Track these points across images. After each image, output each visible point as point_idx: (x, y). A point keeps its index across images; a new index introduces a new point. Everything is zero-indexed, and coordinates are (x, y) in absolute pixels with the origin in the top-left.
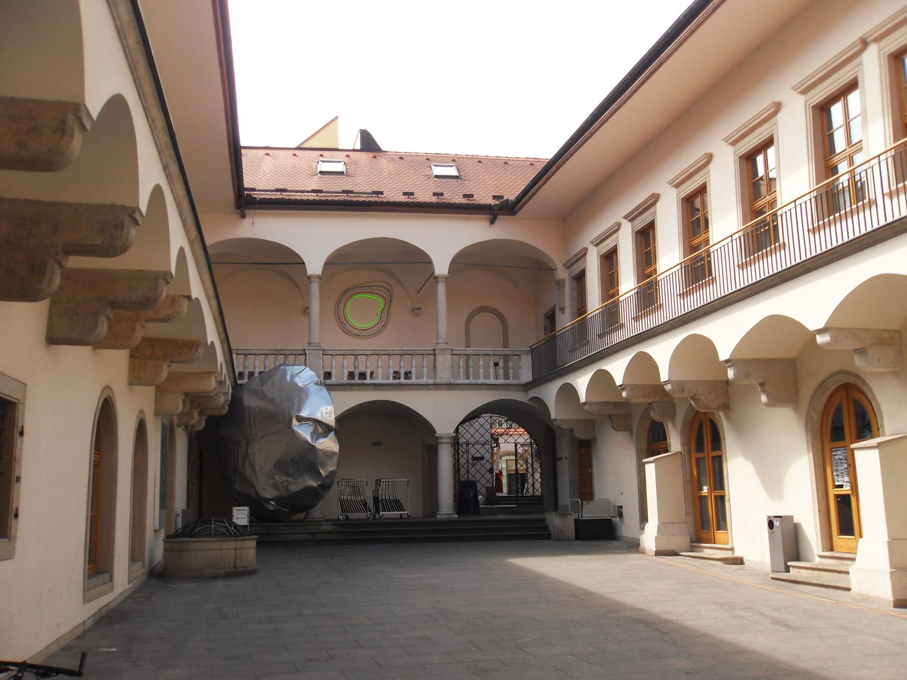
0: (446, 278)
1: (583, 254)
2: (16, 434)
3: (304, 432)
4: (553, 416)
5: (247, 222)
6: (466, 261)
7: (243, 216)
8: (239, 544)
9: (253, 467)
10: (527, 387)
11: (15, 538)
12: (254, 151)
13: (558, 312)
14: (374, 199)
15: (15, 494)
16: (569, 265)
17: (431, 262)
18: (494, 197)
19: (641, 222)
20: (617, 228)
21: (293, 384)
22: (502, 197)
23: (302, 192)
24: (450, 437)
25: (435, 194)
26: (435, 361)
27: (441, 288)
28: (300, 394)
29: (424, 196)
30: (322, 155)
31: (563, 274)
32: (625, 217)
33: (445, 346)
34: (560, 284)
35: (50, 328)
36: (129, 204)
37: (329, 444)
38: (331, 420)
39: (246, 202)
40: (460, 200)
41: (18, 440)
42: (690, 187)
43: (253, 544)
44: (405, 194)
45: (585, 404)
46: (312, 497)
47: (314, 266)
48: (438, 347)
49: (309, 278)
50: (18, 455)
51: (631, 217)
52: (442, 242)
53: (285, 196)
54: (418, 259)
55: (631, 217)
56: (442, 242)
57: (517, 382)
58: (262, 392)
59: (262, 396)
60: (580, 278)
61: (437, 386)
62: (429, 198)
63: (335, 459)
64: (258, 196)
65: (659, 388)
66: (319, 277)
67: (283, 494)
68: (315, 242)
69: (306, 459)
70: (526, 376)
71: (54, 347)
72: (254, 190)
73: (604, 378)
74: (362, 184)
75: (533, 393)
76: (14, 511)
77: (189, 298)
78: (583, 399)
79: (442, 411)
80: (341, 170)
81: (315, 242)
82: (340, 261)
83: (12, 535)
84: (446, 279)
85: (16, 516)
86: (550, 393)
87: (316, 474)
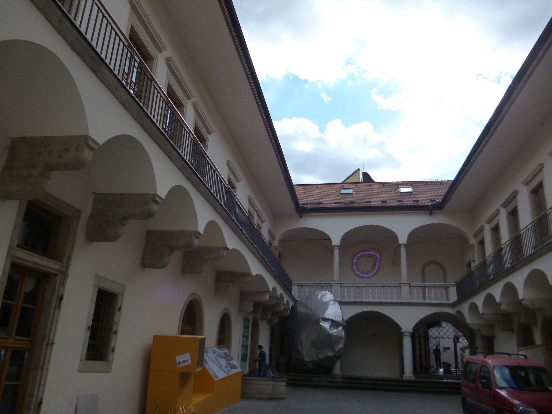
0: (405, 245)
1: (482, 229)
2: (117, 310)
3: (326, 325)
4: (468, 322)
5: (303, 220)
6: (415, 236)
7: (301, 217)
8: (275, 383)
9: (301, 344)
10: (454, 305)
11: (112, 362)
12: (311, 186)
13: (472, 262)
14: (366, 205)
15: (113, 340)
16: (476, 236)
17: (397, 237)
18: (431, 201)
19: (510, 207)
20: (497, 213)
21: (321, 300)
22: (435, 201)
23: (330, 204)
24: (410, 333)
25: (398, 201)
26: (400, 290)
27: (403, 251)
28: (325, 305)
29: (392, 203)
30: (343, 186)
31: (473, 241)
32: (502, 206)
33: (406, 282)
34: (472, 246)
35: (143, 258)
36: (151, 192)
37: (338, 331)
38: (339, 319)
39: (302, 211)
40: (412, 204)
41: (117, 314)
42: (534, 184)
43: (284, 383)
44: (382, 202)
45: (483, 314)
46: (332, 361)
47: (336, 241)
48: (402, 282)
49: (334, 246)
50: (116, 319)
51: (504, 205)
52: (402, 227)
53: (321, 206)
54: (391, 236)
55: (504, 205)
56: (402, 227)
57: (448, 302)
58: (307, 305)
59: (306, 306)
60: (482, 243)
61: (402, 304)
62: (395, 204)
63: (343, 341)
64: (307, 207)
65: (519, 303)
66: (338, 246)
67: (316, 359)
68: (336, 228)
69: (327, 340)
70: (453, 298)
71: (147, 270)
72: (306, 204)
73: (490, 298)
74: (360, 200)
75: (458, 308)
76: (112, 347)
77: (226, 248)
78: (481, 311)
79: (407, 319)
80: (351, 192)
81: (336, 228)
82: (349, 238)
83: (110, 360)
84: (406, 246)
85: (113, 351)
86: (465, 308)
87: (333, 349)
